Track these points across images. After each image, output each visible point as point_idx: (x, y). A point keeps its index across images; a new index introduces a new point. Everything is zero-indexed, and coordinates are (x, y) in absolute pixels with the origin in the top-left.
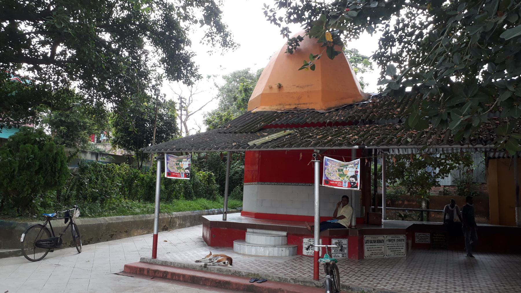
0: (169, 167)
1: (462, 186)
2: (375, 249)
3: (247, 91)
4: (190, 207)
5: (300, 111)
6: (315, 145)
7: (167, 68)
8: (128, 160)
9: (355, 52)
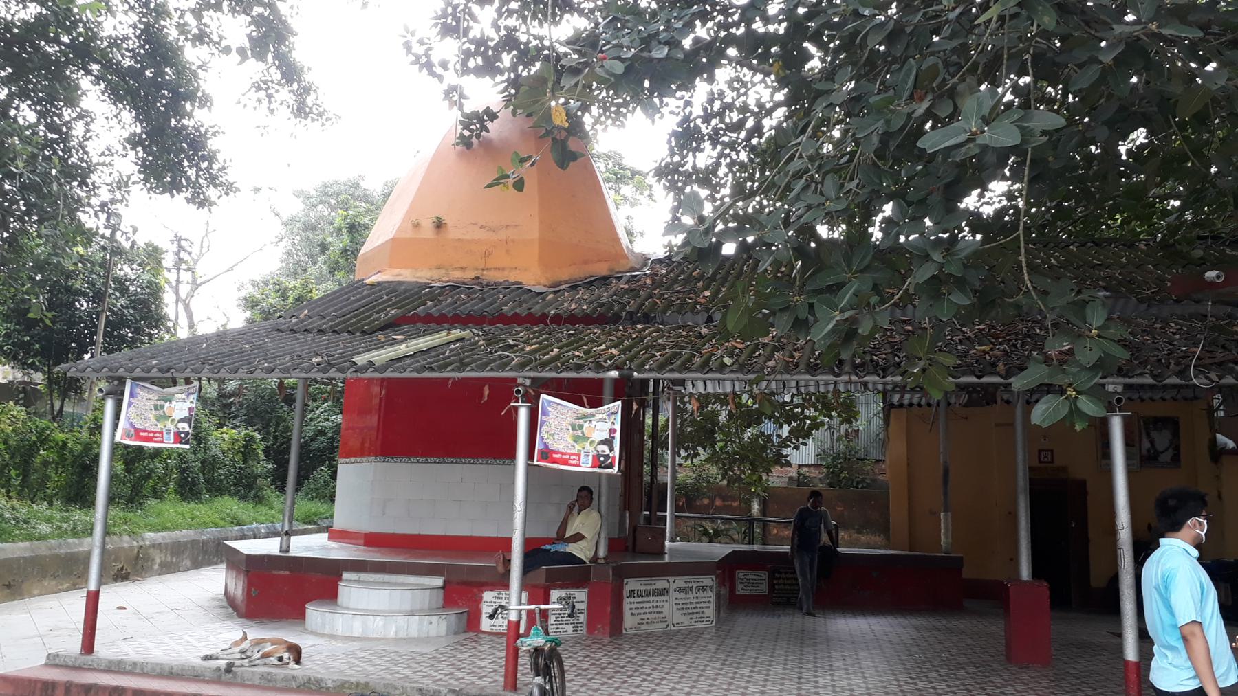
1: (835, 466)
2: (648, 611)
3: (356, 230)
4: (193, 519)
6: (522, 366)
7: (144, 160)
8: (22, 396)
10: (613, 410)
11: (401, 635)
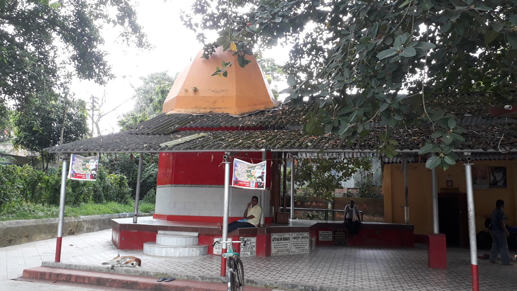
2: (281, 246)
3: (164, 93)
4: (99, 211)
5: (215, 115)
6: (226, 147)
7: (78, 66)
9: (271, 61)
10: (263, 164)
11: (181, 256)
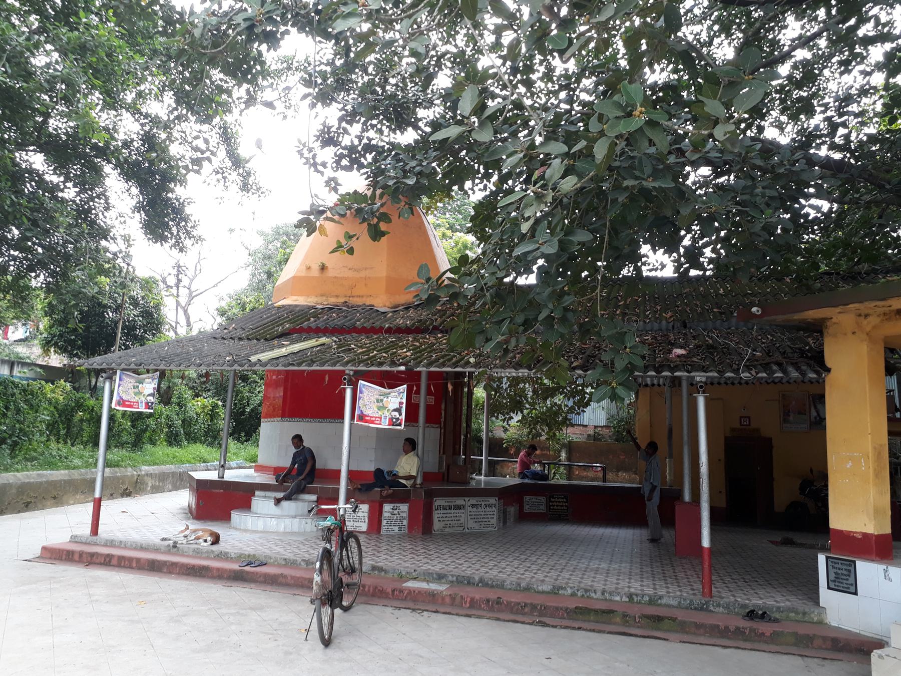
0: (121, 392)
2: (450, 519)
4: (174, 458)
5: (352, 307)
6: (347, 363)
8: (70, 375)
10: (401, 391)
11: (287, 530)
